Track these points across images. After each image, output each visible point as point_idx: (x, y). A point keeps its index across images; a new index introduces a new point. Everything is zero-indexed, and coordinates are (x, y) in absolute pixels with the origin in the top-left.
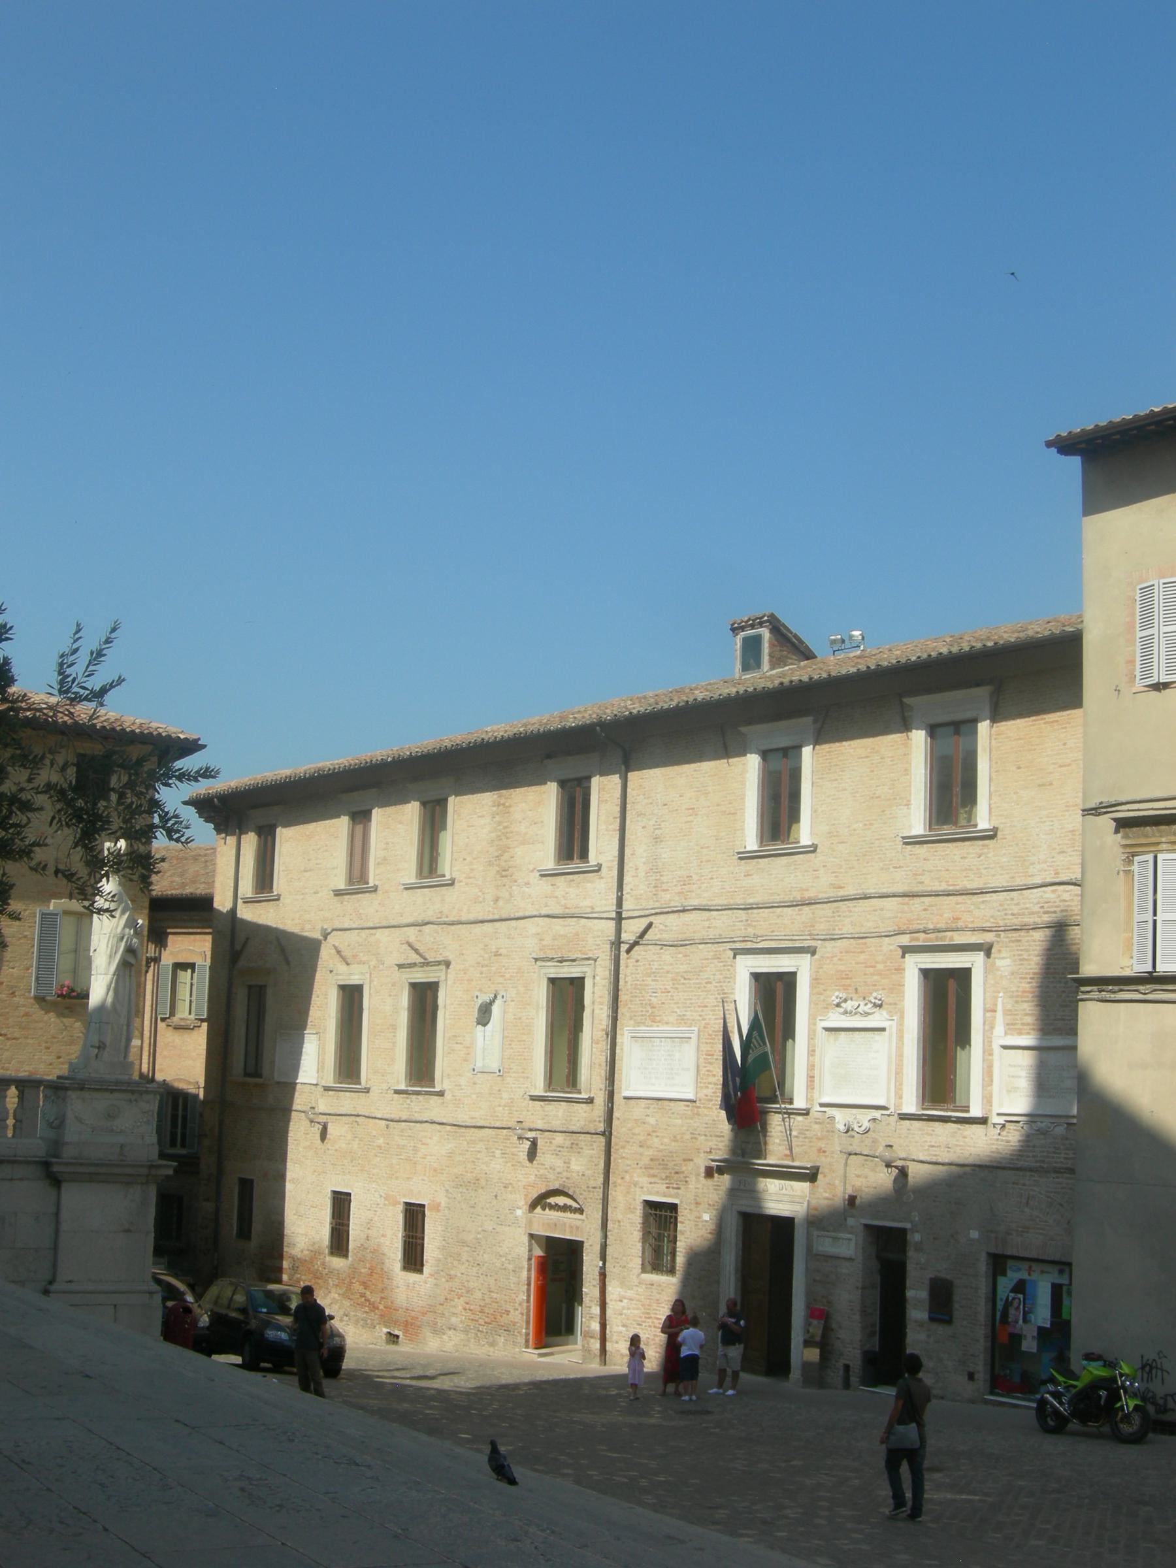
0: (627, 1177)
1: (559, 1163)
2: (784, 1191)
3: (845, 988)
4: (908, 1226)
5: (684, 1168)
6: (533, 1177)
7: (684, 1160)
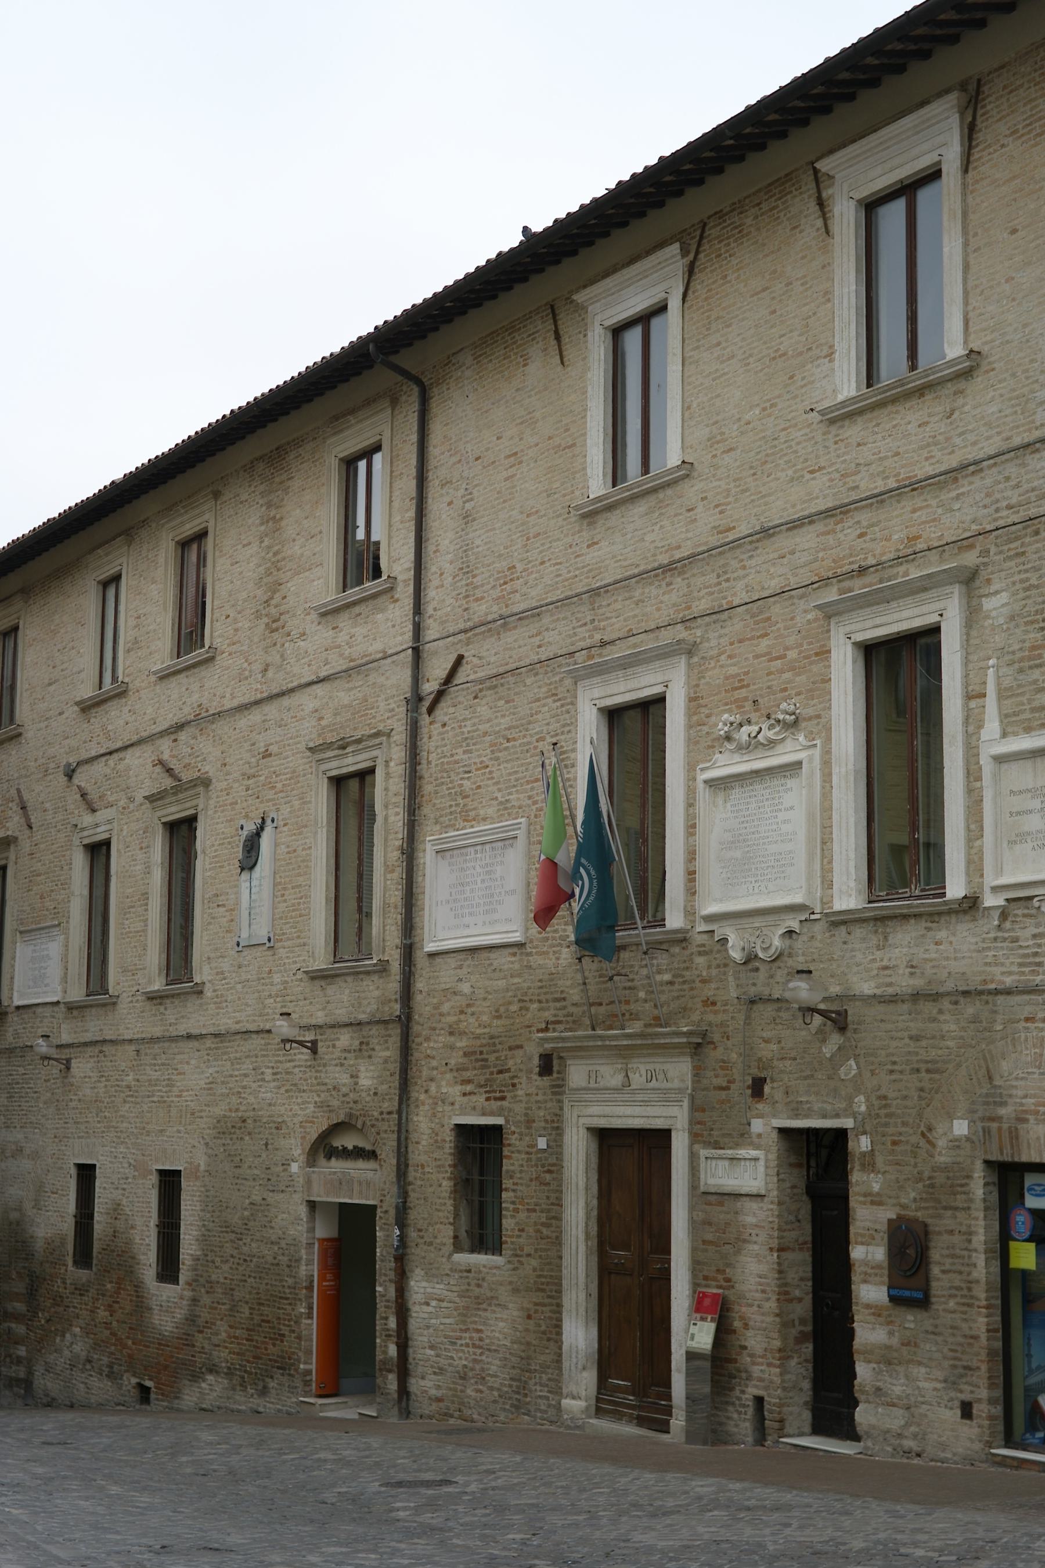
0: (433, 1088)
3: (739, 703)
4: (848, 1123)
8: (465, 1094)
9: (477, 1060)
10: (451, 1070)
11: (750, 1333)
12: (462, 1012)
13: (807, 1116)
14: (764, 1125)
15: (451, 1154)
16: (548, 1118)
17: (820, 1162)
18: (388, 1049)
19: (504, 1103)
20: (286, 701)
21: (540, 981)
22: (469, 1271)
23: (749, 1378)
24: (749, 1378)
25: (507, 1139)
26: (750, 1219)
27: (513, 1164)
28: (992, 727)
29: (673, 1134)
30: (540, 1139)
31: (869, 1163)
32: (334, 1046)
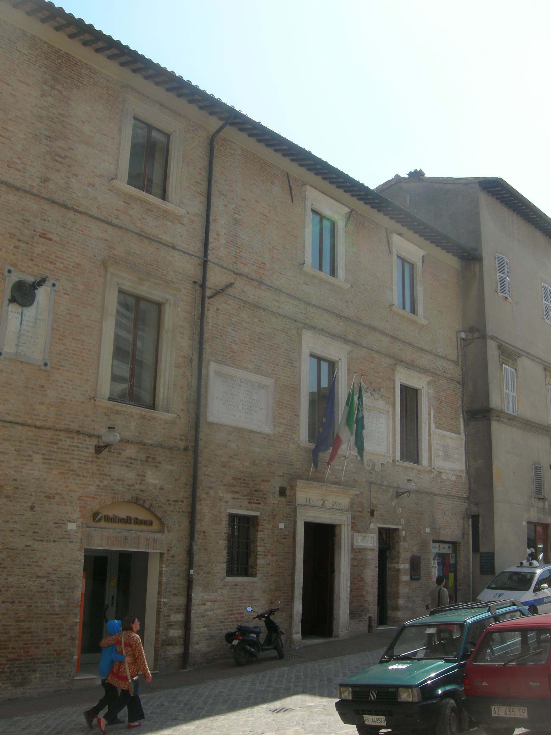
0: (212, 492)
1: (130, 476)
2: (335, 507)
5: (262, 487)
6: (93, 488)
7: (263, 481)
8: (234, 498)
9: (242, 483)
10: (225, 485)
11: (368, 596)
12: (231, 457)
13: (388, 524)
14: (374, 526)
15: (226, 527)
16: (285, 515)
17: (388, 540)
18: (174, 465)
19: (259, 505)
20: (71, 214)
21: (280, 454)
22: (237, 585)
23: (368, 611)
24: (368, 611)
25: (261, 522)
26: (369, 557)
27: (264, 534)
28: (433, 426)
29: (343, 527)
30: (280, 524)
31: (405, 540)
32: (120, 454)
